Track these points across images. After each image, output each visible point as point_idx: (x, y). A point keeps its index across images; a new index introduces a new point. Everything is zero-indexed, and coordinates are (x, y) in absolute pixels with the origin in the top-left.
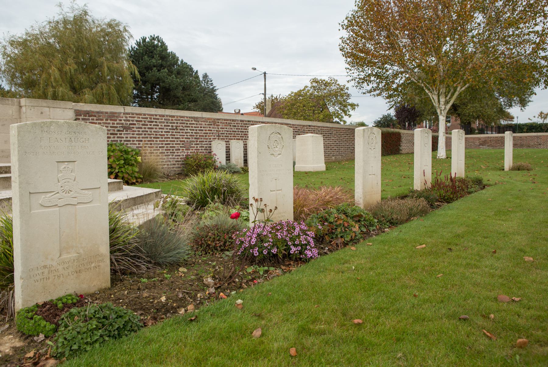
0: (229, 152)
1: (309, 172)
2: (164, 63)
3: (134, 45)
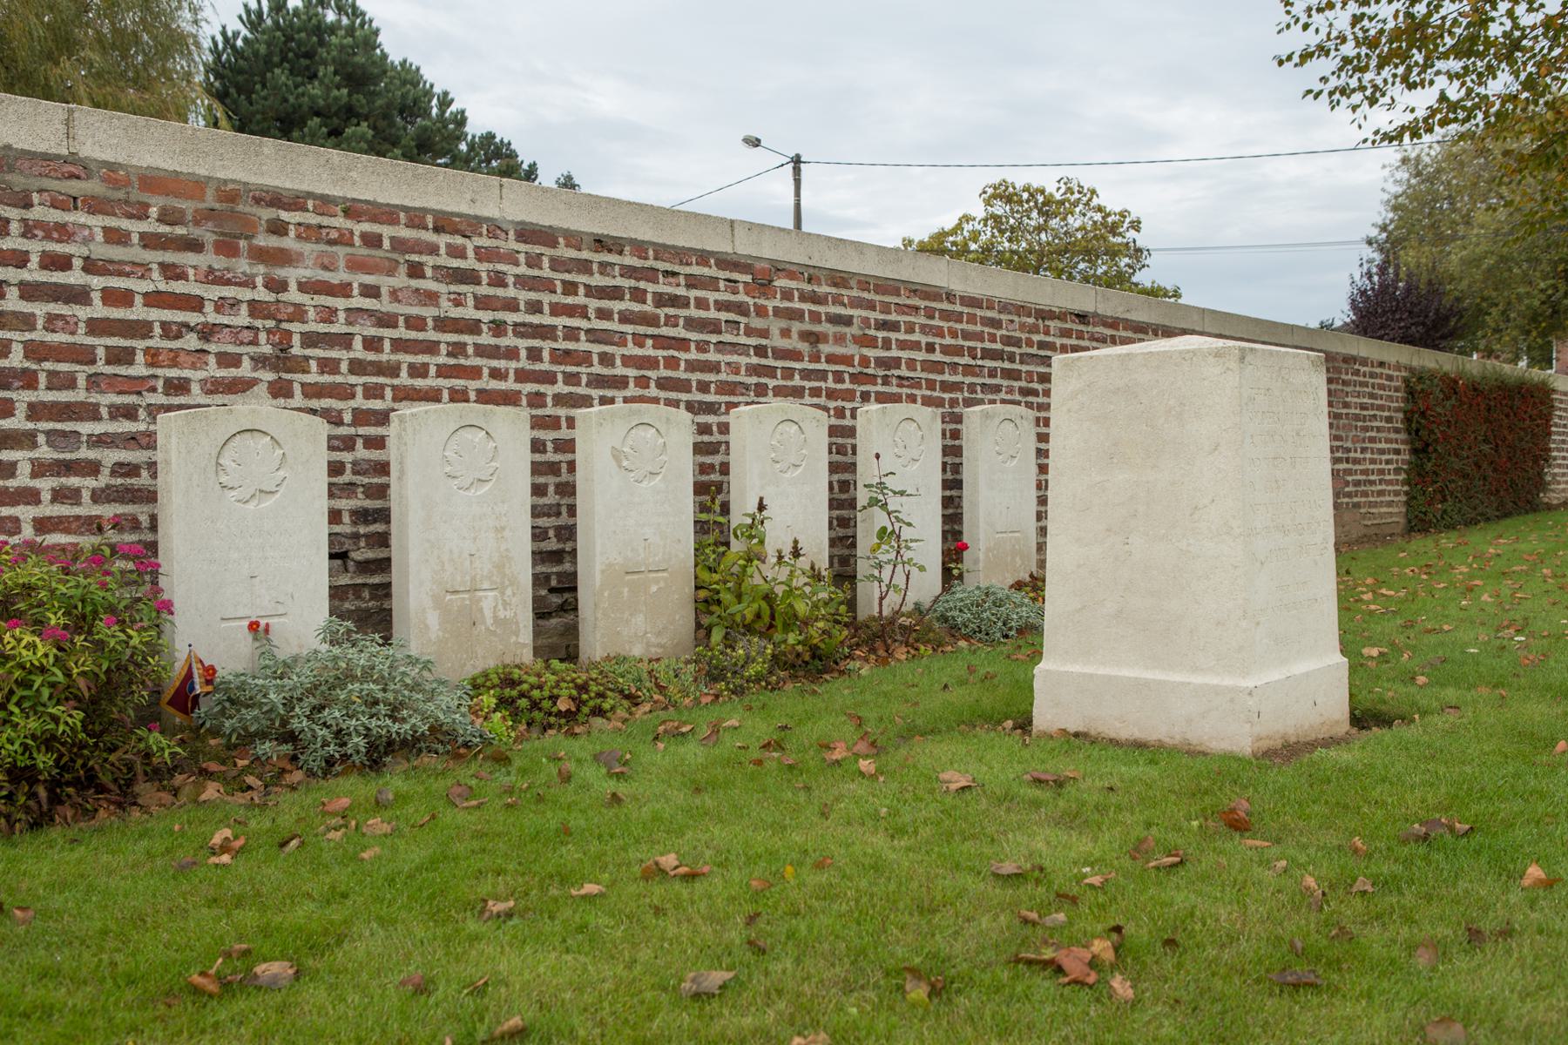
0: (719, 487)
1: (1160, 746)
2: (360, 100)
3: (234, 25)
